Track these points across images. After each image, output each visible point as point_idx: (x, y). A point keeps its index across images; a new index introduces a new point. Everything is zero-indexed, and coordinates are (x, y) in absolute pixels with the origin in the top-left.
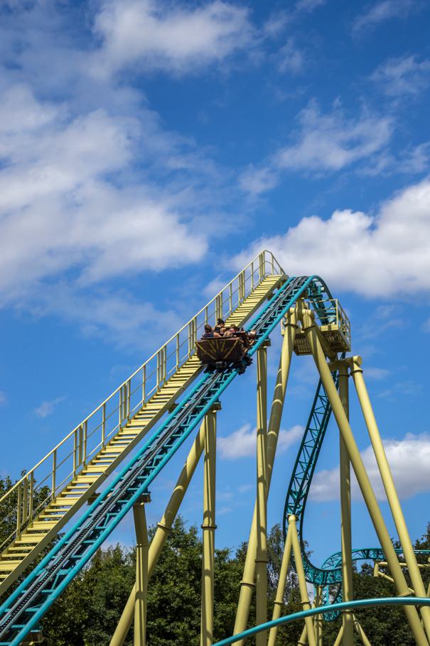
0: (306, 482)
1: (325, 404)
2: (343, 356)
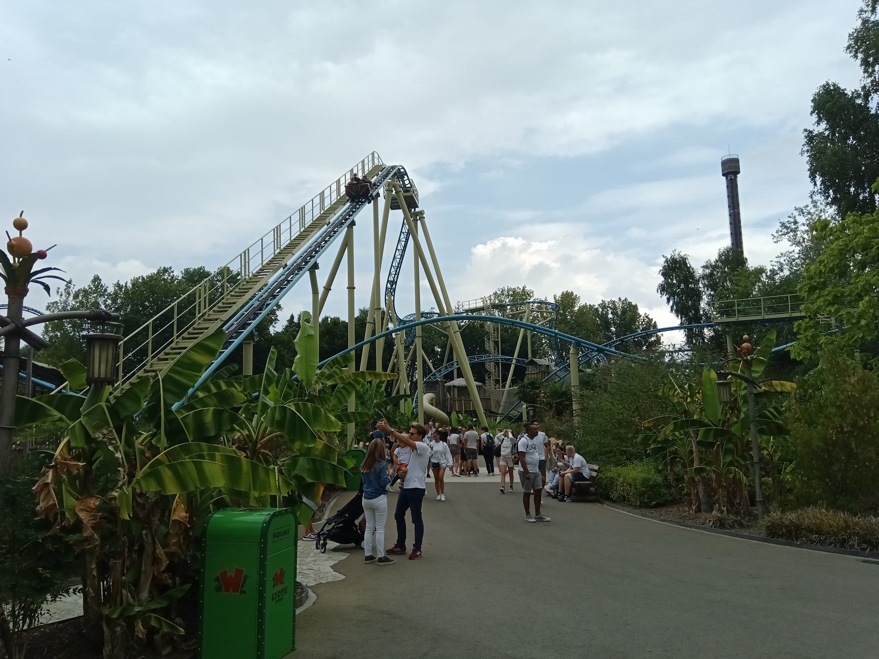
0: (396, 276)
1: (405, 236)
2: (415, 210)
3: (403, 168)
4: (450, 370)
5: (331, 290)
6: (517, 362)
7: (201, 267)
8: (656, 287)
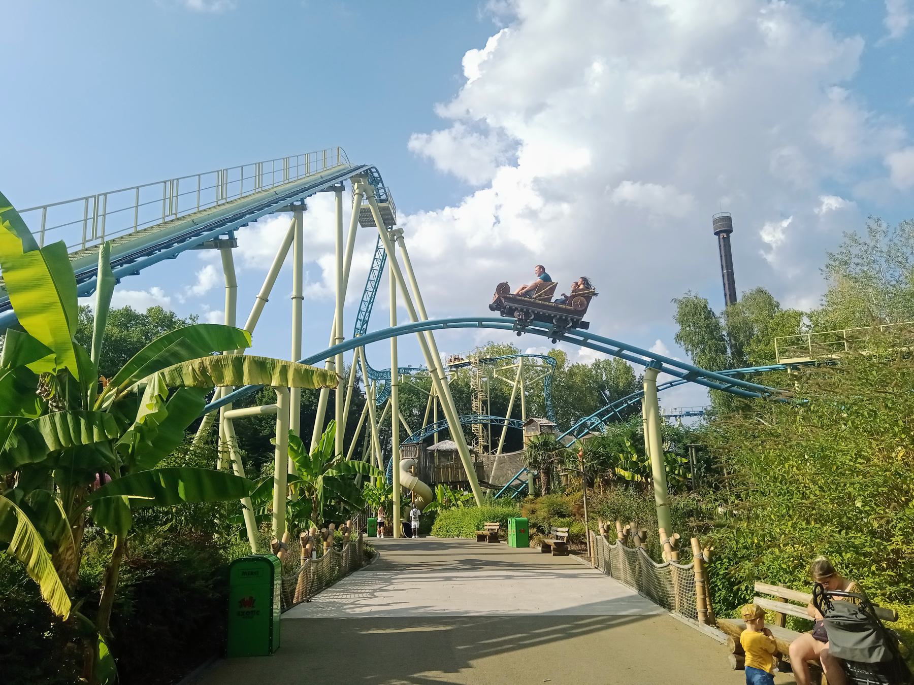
3: (377, 171)
4: (430, 433)
5: (267, 301)
6: (509, 424)
7: (126, 307)
8: (760, 286)
